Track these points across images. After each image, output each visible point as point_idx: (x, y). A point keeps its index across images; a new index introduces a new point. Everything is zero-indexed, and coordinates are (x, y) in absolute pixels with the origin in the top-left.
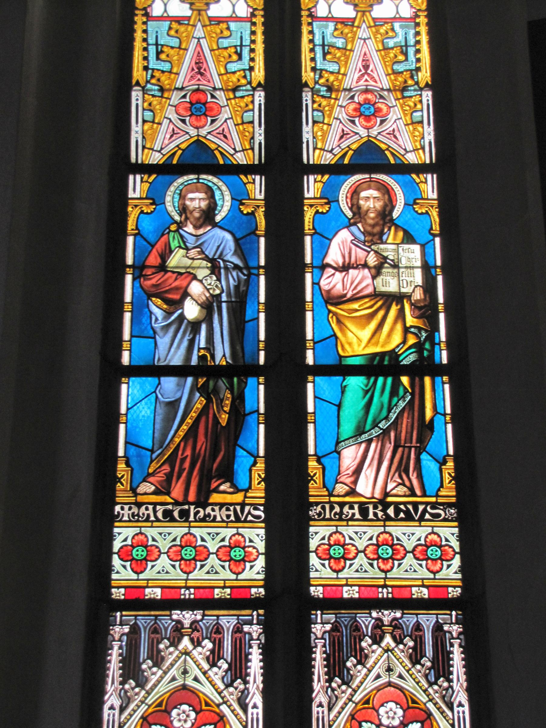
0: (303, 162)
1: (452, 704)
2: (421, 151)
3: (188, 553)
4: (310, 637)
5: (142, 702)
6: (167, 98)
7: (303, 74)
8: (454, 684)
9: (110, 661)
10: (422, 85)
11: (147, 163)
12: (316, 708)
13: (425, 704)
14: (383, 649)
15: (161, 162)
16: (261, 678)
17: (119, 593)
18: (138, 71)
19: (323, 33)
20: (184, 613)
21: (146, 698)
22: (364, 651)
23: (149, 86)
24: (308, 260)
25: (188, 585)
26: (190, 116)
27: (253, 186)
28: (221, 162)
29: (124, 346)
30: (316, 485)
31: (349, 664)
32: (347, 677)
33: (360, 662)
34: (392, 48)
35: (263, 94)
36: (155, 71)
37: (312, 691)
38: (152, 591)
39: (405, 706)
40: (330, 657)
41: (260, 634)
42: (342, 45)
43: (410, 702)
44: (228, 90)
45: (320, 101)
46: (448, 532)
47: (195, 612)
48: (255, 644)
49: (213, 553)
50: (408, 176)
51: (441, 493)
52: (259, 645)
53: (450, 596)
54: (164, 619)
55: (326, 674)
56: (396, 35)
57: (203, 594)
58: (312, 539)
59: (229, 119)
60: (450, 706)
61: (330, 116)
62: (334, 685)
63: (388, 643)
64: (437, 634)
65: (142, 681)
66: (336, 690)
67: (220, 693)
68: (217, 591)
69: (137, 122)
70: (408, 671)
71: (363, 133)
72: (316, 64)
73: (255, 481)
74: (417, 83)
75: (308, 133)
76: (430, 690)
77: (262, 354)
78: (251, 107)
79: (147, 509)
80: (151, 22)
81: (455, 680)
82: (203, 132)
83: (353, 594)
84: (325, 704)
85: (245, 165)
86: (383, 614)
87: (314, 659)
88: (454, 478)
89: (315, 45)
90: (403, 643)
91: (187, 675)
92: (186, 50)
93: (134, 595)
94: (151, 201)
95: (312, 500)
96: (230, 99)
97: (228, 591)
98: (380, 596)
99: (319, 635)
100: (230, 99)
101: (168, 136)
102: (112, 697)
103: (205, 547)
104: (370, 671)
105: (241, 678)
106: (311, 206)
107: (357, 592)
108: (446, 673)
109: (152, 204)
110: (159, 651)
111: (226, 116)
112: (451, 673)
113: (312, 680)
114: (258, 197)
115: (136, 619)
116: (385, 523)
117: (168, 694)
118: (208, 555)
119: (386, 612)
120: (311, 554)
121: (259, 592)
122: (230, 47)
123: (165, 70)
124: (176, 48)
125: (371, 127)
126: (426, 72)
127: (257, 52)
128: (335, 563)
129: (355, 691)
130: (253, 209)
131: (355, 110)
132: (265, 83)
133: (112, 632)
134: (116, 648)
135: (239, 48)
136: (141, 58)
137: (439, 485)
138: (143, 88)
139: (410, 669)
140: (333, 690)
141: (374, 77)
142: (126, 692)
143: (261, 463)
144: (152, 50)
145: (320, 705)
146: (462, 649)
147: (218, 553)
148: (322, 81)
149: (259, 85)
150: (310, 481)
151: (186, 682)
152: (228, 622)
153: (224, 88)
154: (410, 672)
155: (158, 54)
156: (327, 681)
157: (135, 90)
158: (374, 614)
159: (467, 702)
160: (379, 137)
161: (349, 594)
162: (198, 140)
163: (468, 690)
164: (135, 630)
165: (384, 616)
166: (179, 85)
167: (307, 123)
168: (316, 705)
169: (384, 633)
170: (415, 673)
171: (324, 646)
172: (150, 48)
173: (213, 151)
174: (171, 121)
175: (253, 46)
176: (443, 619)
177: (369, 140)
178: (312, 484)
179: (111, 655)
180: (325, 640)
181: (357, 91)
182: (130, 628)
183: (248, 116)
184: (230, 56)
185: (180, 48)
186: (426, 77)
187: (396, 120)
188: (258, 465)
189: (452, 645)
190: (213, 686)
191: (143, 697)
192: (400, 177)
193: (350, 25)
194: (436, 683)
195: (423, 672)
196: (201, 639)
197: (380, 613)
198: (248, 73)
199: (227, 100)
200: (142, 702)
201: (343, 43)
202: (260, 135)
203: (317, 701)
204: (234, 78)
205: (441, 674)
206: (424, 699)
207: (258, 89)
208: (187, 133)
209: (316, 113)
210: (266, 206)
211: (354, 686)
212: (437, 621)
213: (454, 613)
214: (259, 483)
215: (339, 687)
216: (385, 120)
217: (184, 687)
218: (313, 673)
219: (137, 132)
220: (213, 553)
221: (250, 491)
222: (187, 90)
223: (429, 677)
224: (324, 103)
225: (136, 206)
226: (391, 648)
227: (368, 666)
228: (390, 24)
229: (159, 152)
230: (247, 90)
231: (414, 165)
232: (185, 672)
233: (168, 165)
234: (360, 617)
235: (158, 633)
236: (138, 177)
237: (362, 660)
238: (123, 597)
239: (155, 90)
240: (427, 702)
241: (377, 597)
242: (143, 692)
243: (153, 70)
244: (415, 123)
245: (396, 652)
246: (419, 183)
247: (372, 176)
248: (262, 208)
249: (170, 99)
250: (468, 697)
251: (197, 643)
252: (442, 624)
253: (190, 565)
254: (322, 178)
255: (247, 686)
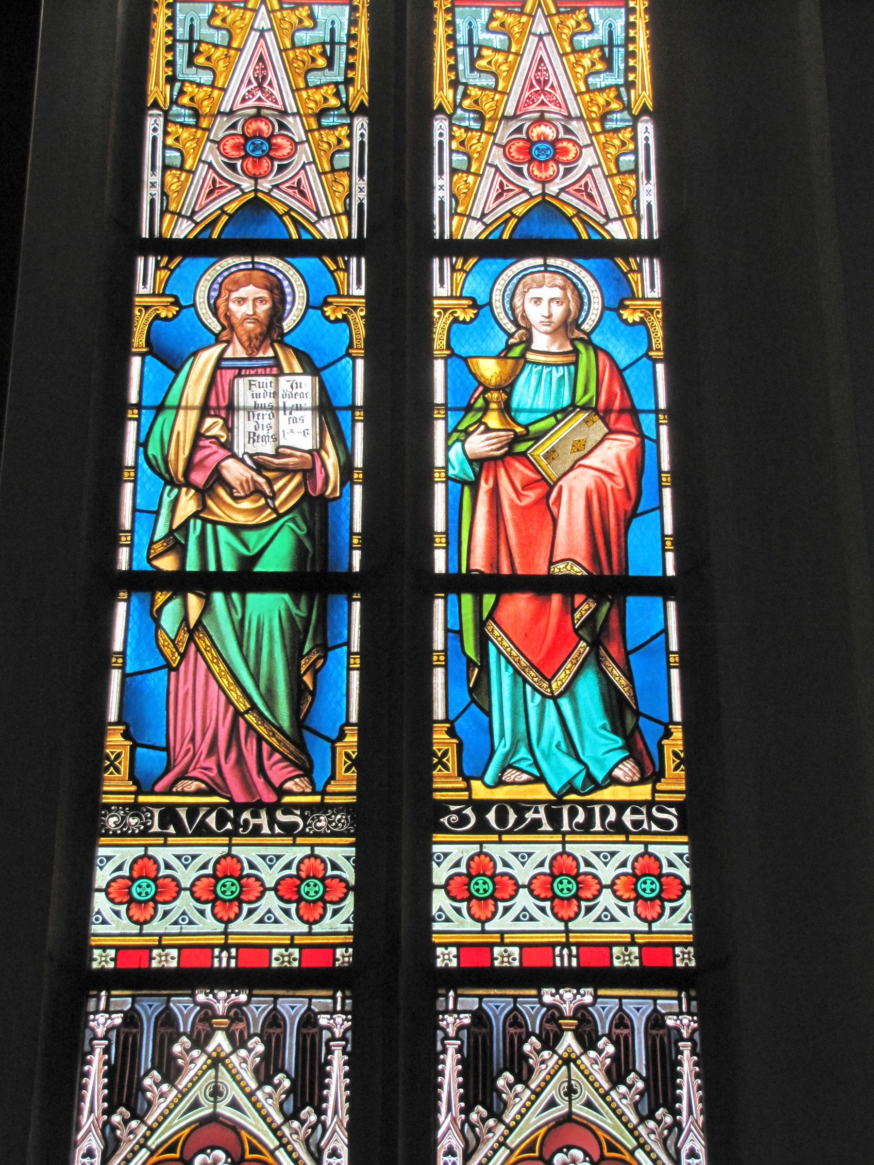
0: (140, 235)
1: (320, 1151)
2: (344, 218)
3: (228, 889)
4: (435, 1035)
5: (502, 1144)
6: (204, 130)
7: (436, 91)
8: (328, 1118)
9: (87, 1075)
10: (354, 107)
11: (459, 238)
12: (80, 1159)
13: (632, 1153)
14: (209, 1056)
15: (483, 237)
16: (700, 1106)
17: (448, 954)
18: (157, 84)
19: (610, 26)
20: (561, 991)
21: (506, 1138)
22: (527, 1062)
23: (175, 109)
24: (439, 398)
25: (164, 942)
26: (243, 158)
27: (639, 276)
28: (585, 236)
29: (437, 540)
30: (446, 772)
31: (501, 1083)
32: (498, 1106)
33: (519, 1080)
34: (588, 50)
35: (650, 127)
36: (187, 84)
37: (437, 1126)
38: (506, 951)
39: (596, 1158)
40: (115, 1073)
41: (694, 1031)
42: (502, 45)
43: (605, 1150)
44: (308, 116)
45: (177, 132)
46: (340, 855)
47: (582, 991)
48: (686, 1047)
49: (185, 889)
50: (317, 260)
51: (330, 788)
52: (344, 1048)
53: (337, 964)
54: (179, 1002)
55: (462, 1098)
56: (593, 29)
57: (253, 961)
58: (101, 868)
59: (309, 163)
60: (317, 1155)
61: (480, 159)
62: (474, 1117)
63: (219, 1045)
64: (304, 1031)
65: (142, 1108)
66: (118, 1128)
67: (631, 1131)
68: (276, 952)
69: (441, 172)
70: (603, 1096)
71: (535, 189)
72: (174, 71)
73: (341, 767)
74: (346, 105)
75: (441, 187)
76: (641, 1129)
77: (357, 555)
78: (347, 144)
79: (537, 811)
80: (461, 9)
81: (330, 1112)
82: (265, 185)
83: (631, 961)
84: (459, 1150)
85: (334, 240)
86: (215, 996)
87: (442, 1073)
88: (356, 763)
89: (456, 45)
90: (595, 1048)
91: (574, 1096)
92: (240, 50)
93: (475, 961)
94: (171, 300)
95: (107, 799)
96: (312, 131)
97: (296, 952)
98: (216, 964)
99: (100, 1031)
100: (312, 131)
101: (494, 194)
102: (90, 1137)
103: (174, 879)
104: (538, 1094)
105: (311, 1104)
106: (147, 308)
107: (636, 958)
108: (671, 1102)
109: (172, 304)
110: (173, 1058)
111: (304, 159)
112: (325, 1099)
113: (437, 1110)
114: (649, 294)
115: (515, 1002)
116: (230, 840)
117: (187, 1131)
118: (178, 893)
119: (222, 994)
120: (97, 894)
121: (685, 958)
122: (316, 45)
123: (202, 82)
124: (224, 47)
125: (550, 180)
126: (644, 89)
127: (639, 57)
128: (480, 906)
129: (152, 1130)
130: (642, 315)
131: (236, 147)
132: (654, 107)
133: (443, 1024)
134: (98, 1051)
135: (606, 50)
136: (162, 63)
137: (329, 774)
138: (166, 113)
139: (607, 1093)
140: (472, 1127)
141: (272, 94)
142: (114, 1128)
143: (352, 735)
144: (182, 49)
145: (450, 1152)
146: (346, 1058)
147: (195, 889)
148: (466, 103)
149: (644, 110)
150: (108, 768)
151: (218, 1110)
152: (293, 1008)
153: (585, 117)
154: (608, 1099)
155: (192, 56)
156: (462, 1111)
157: (151, 115)
158: (201, 997)
159: (346, 1149)
160: (564, 196)
161: (624, 961)
162: (256, 197)
163: (352, 1130)
164: (132, 1019)
165: (218, 1001)
166: (226, 107)
167: (441, 172)
168: (82, 1153)
169: (562, 1031)
170: (617, 1099)
171: (107, 1050)
172: (460, 51)
173: (280, 217)
174: (497, 170)
175: (631, 48)
176: (664, 1006)
177: (256, 197)
178: (440, 770)
179: (443, 1062)
180: (110, 1041)
181: (242, 115)
182: (124, 1019)
183: (342, 161)
184: (313, 60)
185: (229, 47)
186: (644, 97)
187: (304, 165)
188: (347, 739)
189: (329, 1051)
190: (264, 1118)
191: (502, 1135)
192: (591, 263)
193: (516, 13)
194: (651, 1116)
195: (629, 1097)
196: (524, 1037)
197: (211, 996)
198: (342, 88)
199: (306, 132)
200: (502, 1144)
201: (501, 40)
202: (361, 190)
203: (82, 1148)
204: (601, 99)
205: (661, 1101)
206: (631, 1143)
207: (644, 118)
208: (238, 186)
209: (455, 157)
210: (666, 307)
211: (150, 1122)
212: (655, 1010)
213: (339, 994)
214: (347, 770)
215: (126, 1122)
216: (286, 166)
217: (569, 1118)
218: (439, 1098)
219: (153, 185)
220: (185, 889)
221: (332, 782)
222: (239, 116)
223: (640, 1107)
224: (185, 134)
225: (445, 310)
226: (222, 1055)
227: (533, 1086)
228: (306, 8)
229: (480, 220)
230: (622, 120)
231: (332, 241)
232: (570, 1091)
233: (205, 240)
234: (175, 1003)
235: (520, 1026)
236: (152, 260)
237: (523, 1074)
238: (111, 965)
239: (185, 116)
240: (277, 1148)
241: (209, 966)
242: (144, 1128)
243: (183, 82)
244: (624, 173)
245: (582, 1063)
246: (335, 271)
247: (256, 260)
248: (362, 310)
249: (495, 135)
250: (349, 1138)
251: (238, 1042)
252: (663, 1015)
253: (486, 906)
254: (464, 263)
255: (323, 1117)
